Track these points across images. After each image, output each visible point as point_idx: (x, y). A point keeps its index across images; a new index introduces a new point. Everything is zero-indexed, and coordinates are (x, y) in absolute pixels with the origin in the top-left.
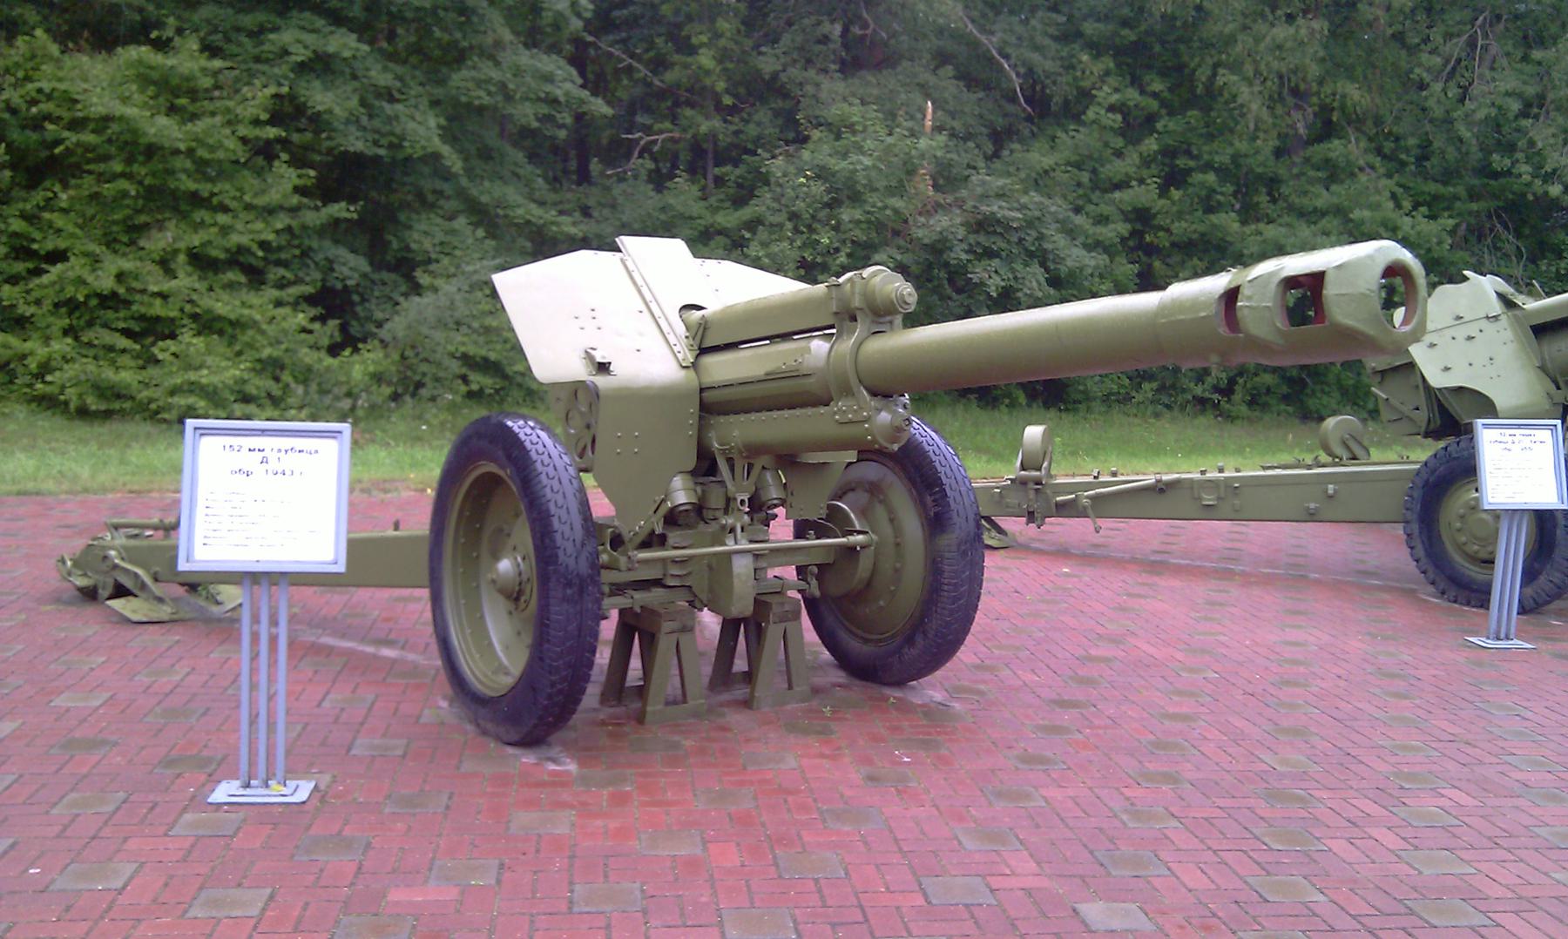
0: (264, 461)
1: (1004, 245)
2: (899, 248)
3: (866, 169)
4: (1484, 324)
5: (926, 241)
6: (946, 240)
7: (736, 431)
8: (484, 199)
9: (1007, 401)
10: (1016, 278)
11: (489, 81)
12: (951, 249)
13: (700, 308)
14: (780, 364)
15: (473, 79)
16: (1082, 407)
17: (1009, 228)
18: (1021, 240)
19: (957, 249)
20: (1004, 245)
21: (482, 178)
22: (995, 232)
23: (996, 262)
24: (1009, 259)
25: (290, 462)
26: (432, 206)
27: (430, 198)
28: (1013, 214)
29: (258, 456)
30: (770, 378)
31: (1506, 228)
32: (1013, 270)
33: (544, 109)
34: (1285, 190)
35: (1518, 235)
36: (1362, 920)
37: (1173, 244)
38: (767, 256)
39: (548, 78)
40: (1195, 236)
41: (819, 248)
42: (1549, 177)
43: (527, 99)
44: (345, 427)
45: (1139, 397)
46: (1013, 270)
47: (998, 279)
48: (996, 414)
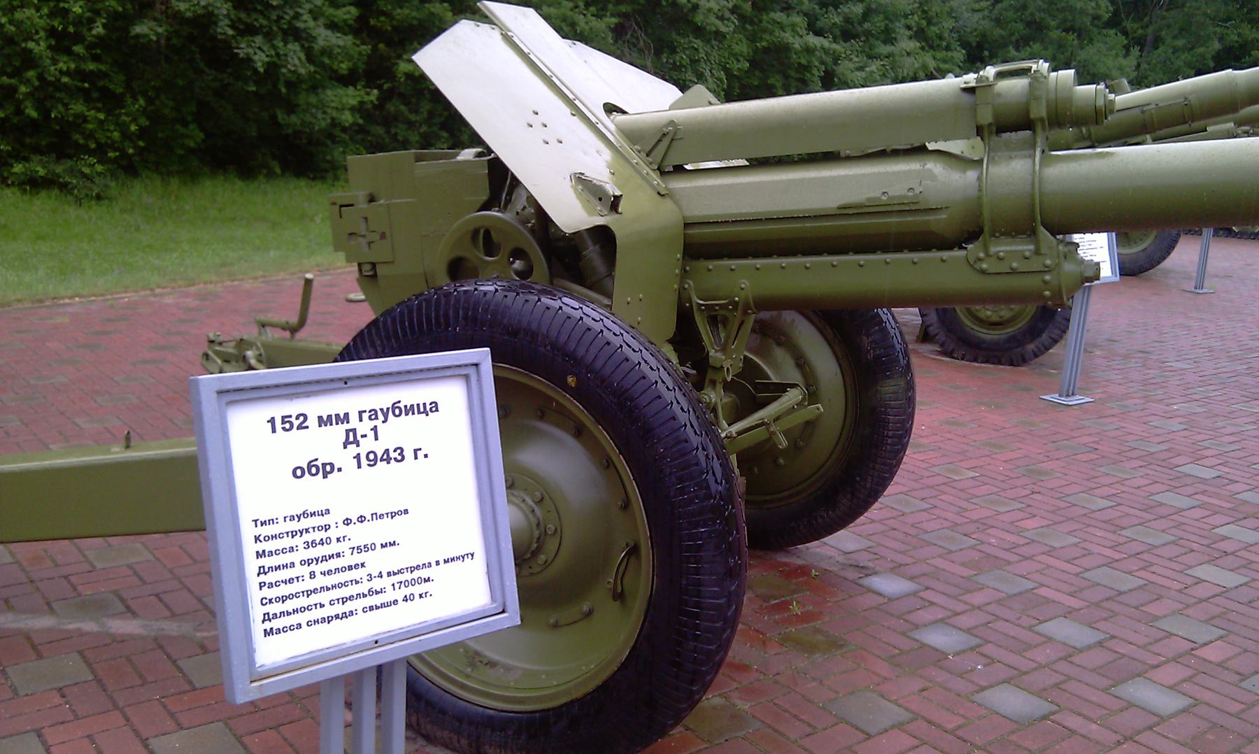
0: (351, 439)
1: (265, 22)
2: (155, 19)
5: (189, 14)
6: (211, 14)
7: (745, 278)
9: (265, 171)
10: (278, 55)
12: (216, 24)
13: (624, 112)
14: (877, 194)
16: (330, 175)
18: (280, 18)
19: (221, 24)
20: (265, 22)
22: (255, 10)
23: (259, 40)
24: (269, 36)
25: (395, 432)
29: (339, 431)
30: (844, 212)
31: (640, 28)
32: (274, 47)
35: (646, 34)
36: (967, 607)
37: (395, 28)
38: (11, 22)
40: (415, 22)
41: (71, 16)
46: (274, 47)
47: (263, 56)
48: (256, 184)
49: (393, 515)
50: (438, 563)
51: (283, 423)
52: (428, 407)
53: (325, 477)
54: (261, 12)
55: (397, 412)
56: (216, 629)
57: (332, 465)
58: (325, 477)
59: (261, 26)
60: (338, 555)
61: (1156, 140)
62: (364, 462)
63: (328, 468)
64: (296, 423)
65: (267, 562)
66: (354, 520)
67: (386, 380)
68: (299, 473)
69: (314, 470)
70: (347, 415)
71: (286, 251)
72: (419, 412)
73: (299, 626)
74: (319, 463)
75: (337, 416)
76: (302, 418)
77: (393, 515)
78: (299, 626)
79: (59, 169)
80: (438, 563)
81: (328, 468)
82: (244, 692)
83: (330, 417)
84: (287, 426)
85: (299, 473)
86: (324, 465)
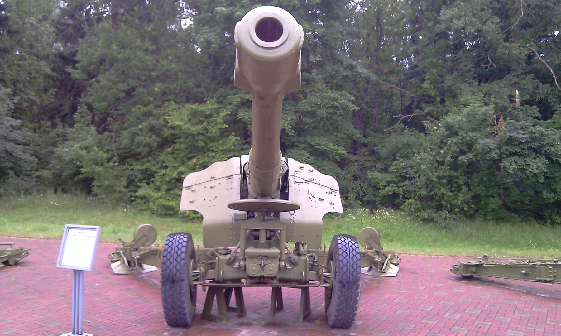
3: (460, 121)
4: (224, 181)
8: (312, 143)
11: (312, 102)
15: (306, 103)
17: (521, 143)
21: (315, 136)
26: (297, 146)
27: (297, 144)
28: (522, 136)
33: (332, 110)
39: (336, 100)
43: (325, 107)
44: (97, 227)
59: (516, 152)
79: (434, 215)
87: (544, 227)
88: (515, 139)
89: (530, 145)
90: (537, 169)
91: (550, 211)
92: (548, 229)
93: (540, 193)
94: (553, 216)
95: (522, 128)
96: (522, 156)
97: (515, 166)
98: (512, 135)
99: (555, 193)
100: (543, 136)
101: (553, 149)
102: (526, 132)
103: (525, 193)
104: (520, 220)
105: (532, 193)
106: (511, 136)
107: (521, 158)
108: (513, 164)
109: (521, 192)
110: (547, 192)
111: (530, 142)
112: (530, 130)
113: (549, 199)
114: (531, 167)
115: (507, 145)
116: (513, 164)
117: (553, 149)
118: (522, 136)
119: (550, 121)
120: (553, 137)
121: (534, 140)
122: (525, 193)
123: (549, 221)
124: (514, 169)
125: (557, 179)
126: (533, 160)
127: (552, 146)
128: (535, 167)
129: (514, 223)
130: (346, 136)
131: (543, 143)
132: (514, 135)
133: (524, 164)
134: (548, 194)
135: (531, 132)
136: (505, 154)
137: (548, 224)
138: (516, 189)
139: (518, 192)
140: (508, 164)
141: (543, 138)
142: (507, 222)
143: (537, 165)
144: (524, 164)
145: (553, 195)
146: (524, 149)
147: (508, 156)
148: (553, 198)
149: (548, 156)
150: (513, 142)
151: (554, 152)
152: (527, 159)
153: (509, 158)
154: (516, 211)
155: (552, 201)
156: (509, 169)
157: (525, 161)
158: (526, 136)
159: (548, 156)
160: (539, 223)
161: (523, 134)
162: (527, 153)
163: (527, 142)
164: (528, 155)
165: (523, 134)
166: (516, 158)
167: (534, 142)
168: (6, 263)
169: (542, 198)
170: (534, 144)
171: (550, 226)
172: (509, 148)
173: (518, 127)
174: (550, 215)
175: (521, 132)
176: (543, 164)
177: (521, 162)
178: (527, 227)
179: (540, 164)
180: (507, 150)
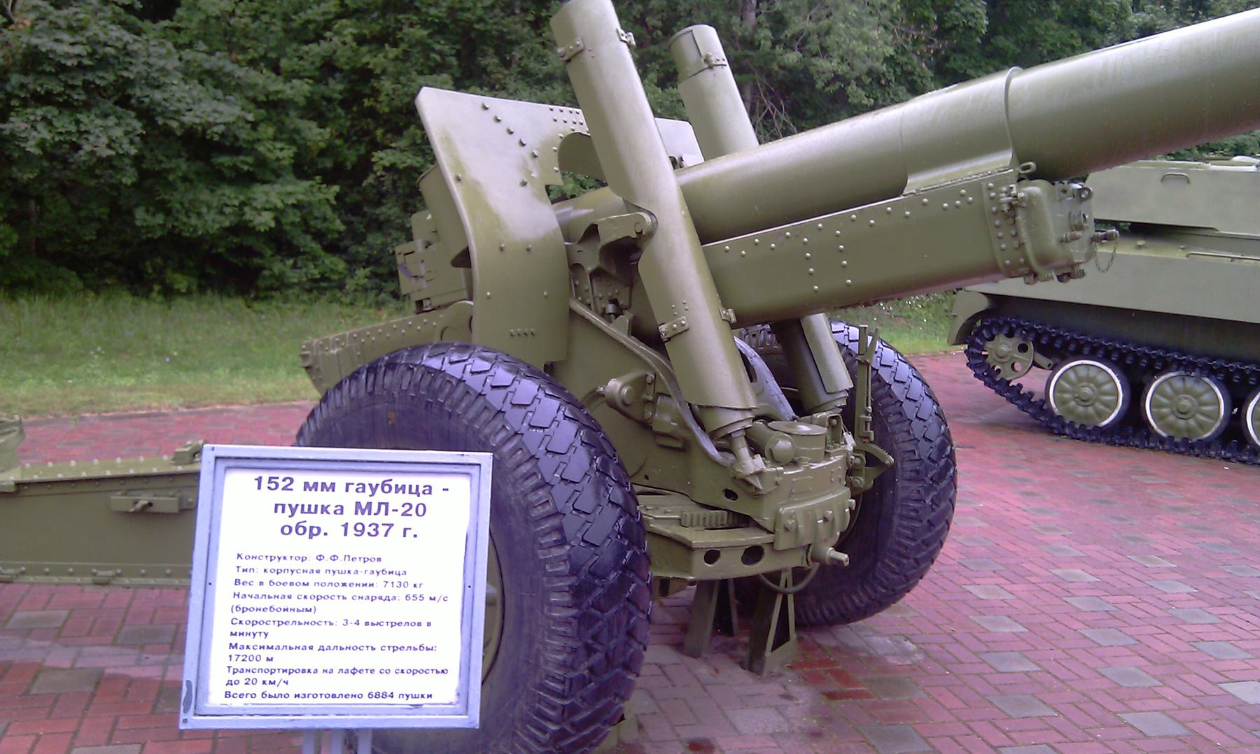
17: (63, 68)
22: (43, 73)
28: (67, 48)
34: (517, 53)
42: (788, 47)
45: (350, 284)
49: (393, 624)
50: (316, 671)
51: (270, 482)
52: (421, 490)
53: (311, 537)
54: (56, 75)
55: (386, 489)
56: (558, 216)
57: (319, 529)
58: (311, 537)
59: (49, 93)
60: (372, 585)
61: (489, 603)
62: (351, 530)
63: (315, 531)
64: (282, 485)
65: (241, 589)
66: (327, 557)
67: (203, 655)
68: (286, 530)
69: (301, 530)
70: (333, 485)
71: (267, 361)
72: (410, 492)
73: (297, 696)
74: (307, 526)
75: (324, 484)
76: (288, 481)
77: (393, 624)
78: (297, 696)
80: (316, 671)
81: (315, 531)
82: (191, 721)
83: (316, 484)
84: (273, 486)
85: (286, 530)
86: (312, 528)
87: (144, 303)
88: (46, 54)
89: (90, 77)
90: (109, 146)
91: (159, 261)
92: (155, 306)
93: (130, 213)
94: (169, 273)
95: (70, 29)
96: (67, 106)
97: (44, 133)
98: (34, 41)
99: (168, 212)
100: (128, 54)
101: (158, 95)
102: (78, 38)
103: (83, 214)
104: (80, 285)
105: (103, 212)
106: (36, 46)
107: (67, 113)
108: (40, 126)
109: (76, 209)
110: (147, 211)
111: (91, 69)
112: (88, 34)
113: (149, 229)
114: (92, 138)
115: (25, 73)
116: (40, 126)
117: (158, 95)
118: (66, 47)
119: (166, 23)
120: (161, 63)
121: (103, 63)
122: (83, 214)
123: (157, 287)
124: (42, 144)
125: (171, 177)
126: (99, 122)
127: (158, 87)
128: (104, 140)
129: (61, 294)
130: (346, 387)
131: (125, 74)
132: (44, 43)
133: (73, 128)
134: (148, 218)
135: (93, 42)
136: (18, 97)
137: (154, 294)
138: (62, 200)
139: (66, 210)
140: (24, 126)
141: (128, 59)
142: (42, 291)
143: (107, 135)
144: (73, 128)
145: (160, 219)
146: (73, 87)
147: (25, 103)
148: (163, 226)
149: (146, 114)
150: (41, 64)
151: (159, 104)
152: (82, 117)
153: (29, 110)
154: (57, 259)
155: (159, 233)
156: (26, 140)
157: (78, 122)
158: (78, 50)
159: (146, 114)
160: (135, 294)
161: (72, 44)
162: (83, 97)
163: (80, 66)
164: (87, 106)
165: (72, 44)
166: (51, 111)
167: (105, 69)
168: (331, 624)
169: (134, 226)
170: (101, 74)
171: (160, 298)
172: (29, 80)
173: (63, 23)
174: (160, 272)
175: (66, 37)
176: (127, 133)
177: (64, 123)
178: (94, 304)
179: (118, 133)
180: (23, 86)
